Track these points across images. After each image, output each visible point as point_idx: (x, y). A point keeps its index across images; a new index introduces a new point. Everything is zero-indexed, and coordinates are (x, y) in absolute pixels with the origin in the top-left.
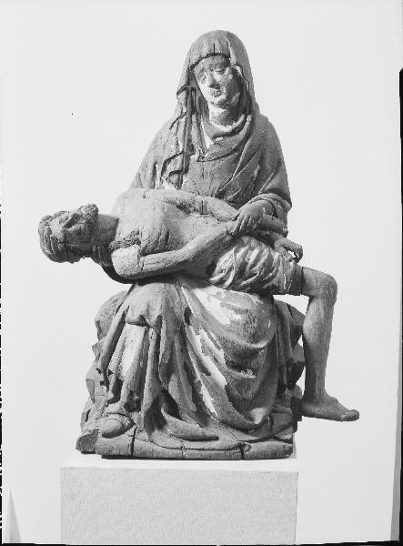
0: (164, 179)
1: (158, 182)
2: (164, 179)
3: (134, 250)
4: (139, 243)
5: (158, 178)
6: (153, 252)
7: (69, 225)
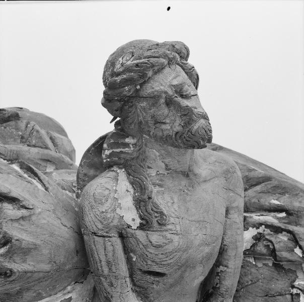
0: (261, 230)
1: (256, 217)
2: (261, 230)
3: (131, 217)
4: (141, 227)
5: (262, 219)
6: (126, 250)
7: (169, 102)
